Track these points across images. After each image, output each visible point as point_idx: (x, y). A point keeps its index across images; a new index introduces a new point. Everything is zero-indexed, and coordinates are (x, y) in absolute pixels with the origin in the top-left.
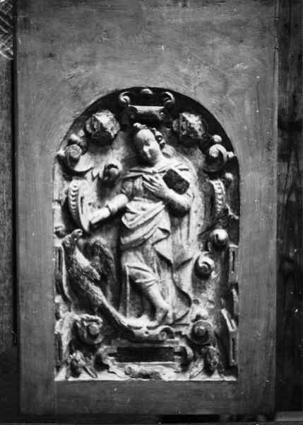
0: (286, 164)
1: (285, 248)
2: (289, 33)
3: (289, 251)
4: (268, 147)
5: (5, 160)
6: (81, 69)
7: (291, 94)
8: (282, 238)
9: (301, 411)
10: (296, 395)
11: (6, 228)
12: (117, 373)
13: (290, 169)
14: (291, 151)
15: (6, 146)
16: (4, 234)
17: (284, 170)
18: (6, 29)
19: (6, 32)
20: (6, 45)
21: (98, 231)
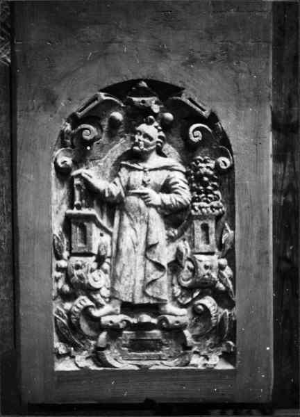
3: (286, 252)
13: (287, 169)
15: (5, 152)
20: (3, 51)
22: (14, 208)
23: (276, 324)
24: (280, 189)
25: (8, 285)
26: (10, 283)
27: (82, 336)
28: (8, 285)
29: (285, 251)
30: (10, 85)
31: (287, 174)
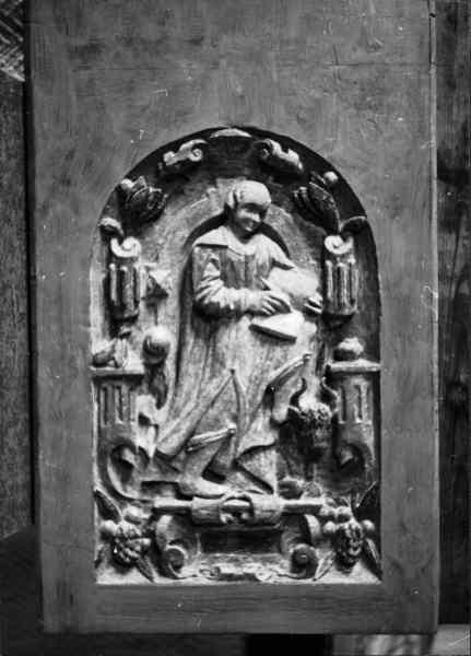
0: (454, 236)
1: (452, 369)
2: (455, 30)
3: (459, 373)
4: (18, 133)
5: (15, 237)
6: (217, 95)
7: (459, 127)
8: (448, 351)
9: (467, 623)
10: (466, 604)
11: (17, 341)
12: (195, 571)
13: (460, 243)
14: (460, 215)
15: (17, 216)
16: (14, 351)
17: (451, 246)
18: (7, 38)
19: (7, 41)
20: (7, 62)
21: (108, 312)
22: (33, 323)
23: (443, 492)
24: (450, 274)
25: (19, 426)
26: (23, 424)
27: (73, 372)
28: (19, 426)
29: (457, 372)
30: (24, 111)
31: (461, 250)
